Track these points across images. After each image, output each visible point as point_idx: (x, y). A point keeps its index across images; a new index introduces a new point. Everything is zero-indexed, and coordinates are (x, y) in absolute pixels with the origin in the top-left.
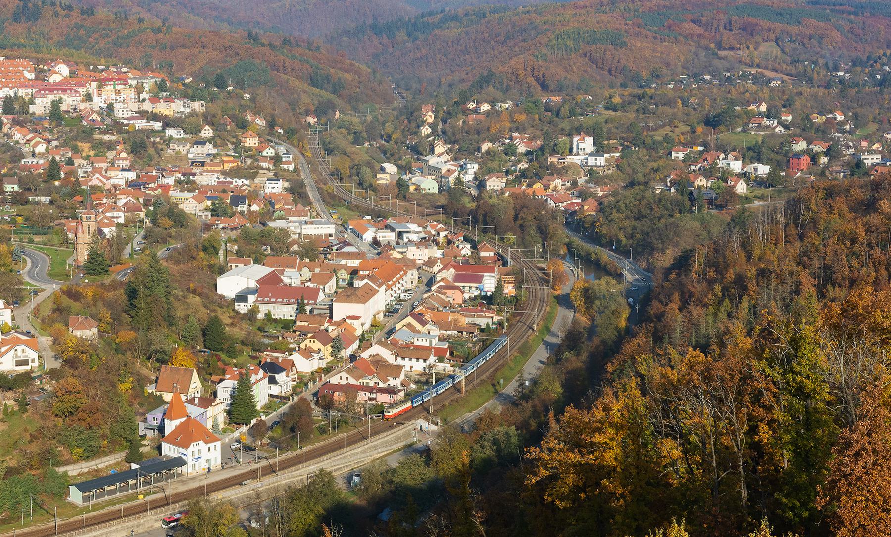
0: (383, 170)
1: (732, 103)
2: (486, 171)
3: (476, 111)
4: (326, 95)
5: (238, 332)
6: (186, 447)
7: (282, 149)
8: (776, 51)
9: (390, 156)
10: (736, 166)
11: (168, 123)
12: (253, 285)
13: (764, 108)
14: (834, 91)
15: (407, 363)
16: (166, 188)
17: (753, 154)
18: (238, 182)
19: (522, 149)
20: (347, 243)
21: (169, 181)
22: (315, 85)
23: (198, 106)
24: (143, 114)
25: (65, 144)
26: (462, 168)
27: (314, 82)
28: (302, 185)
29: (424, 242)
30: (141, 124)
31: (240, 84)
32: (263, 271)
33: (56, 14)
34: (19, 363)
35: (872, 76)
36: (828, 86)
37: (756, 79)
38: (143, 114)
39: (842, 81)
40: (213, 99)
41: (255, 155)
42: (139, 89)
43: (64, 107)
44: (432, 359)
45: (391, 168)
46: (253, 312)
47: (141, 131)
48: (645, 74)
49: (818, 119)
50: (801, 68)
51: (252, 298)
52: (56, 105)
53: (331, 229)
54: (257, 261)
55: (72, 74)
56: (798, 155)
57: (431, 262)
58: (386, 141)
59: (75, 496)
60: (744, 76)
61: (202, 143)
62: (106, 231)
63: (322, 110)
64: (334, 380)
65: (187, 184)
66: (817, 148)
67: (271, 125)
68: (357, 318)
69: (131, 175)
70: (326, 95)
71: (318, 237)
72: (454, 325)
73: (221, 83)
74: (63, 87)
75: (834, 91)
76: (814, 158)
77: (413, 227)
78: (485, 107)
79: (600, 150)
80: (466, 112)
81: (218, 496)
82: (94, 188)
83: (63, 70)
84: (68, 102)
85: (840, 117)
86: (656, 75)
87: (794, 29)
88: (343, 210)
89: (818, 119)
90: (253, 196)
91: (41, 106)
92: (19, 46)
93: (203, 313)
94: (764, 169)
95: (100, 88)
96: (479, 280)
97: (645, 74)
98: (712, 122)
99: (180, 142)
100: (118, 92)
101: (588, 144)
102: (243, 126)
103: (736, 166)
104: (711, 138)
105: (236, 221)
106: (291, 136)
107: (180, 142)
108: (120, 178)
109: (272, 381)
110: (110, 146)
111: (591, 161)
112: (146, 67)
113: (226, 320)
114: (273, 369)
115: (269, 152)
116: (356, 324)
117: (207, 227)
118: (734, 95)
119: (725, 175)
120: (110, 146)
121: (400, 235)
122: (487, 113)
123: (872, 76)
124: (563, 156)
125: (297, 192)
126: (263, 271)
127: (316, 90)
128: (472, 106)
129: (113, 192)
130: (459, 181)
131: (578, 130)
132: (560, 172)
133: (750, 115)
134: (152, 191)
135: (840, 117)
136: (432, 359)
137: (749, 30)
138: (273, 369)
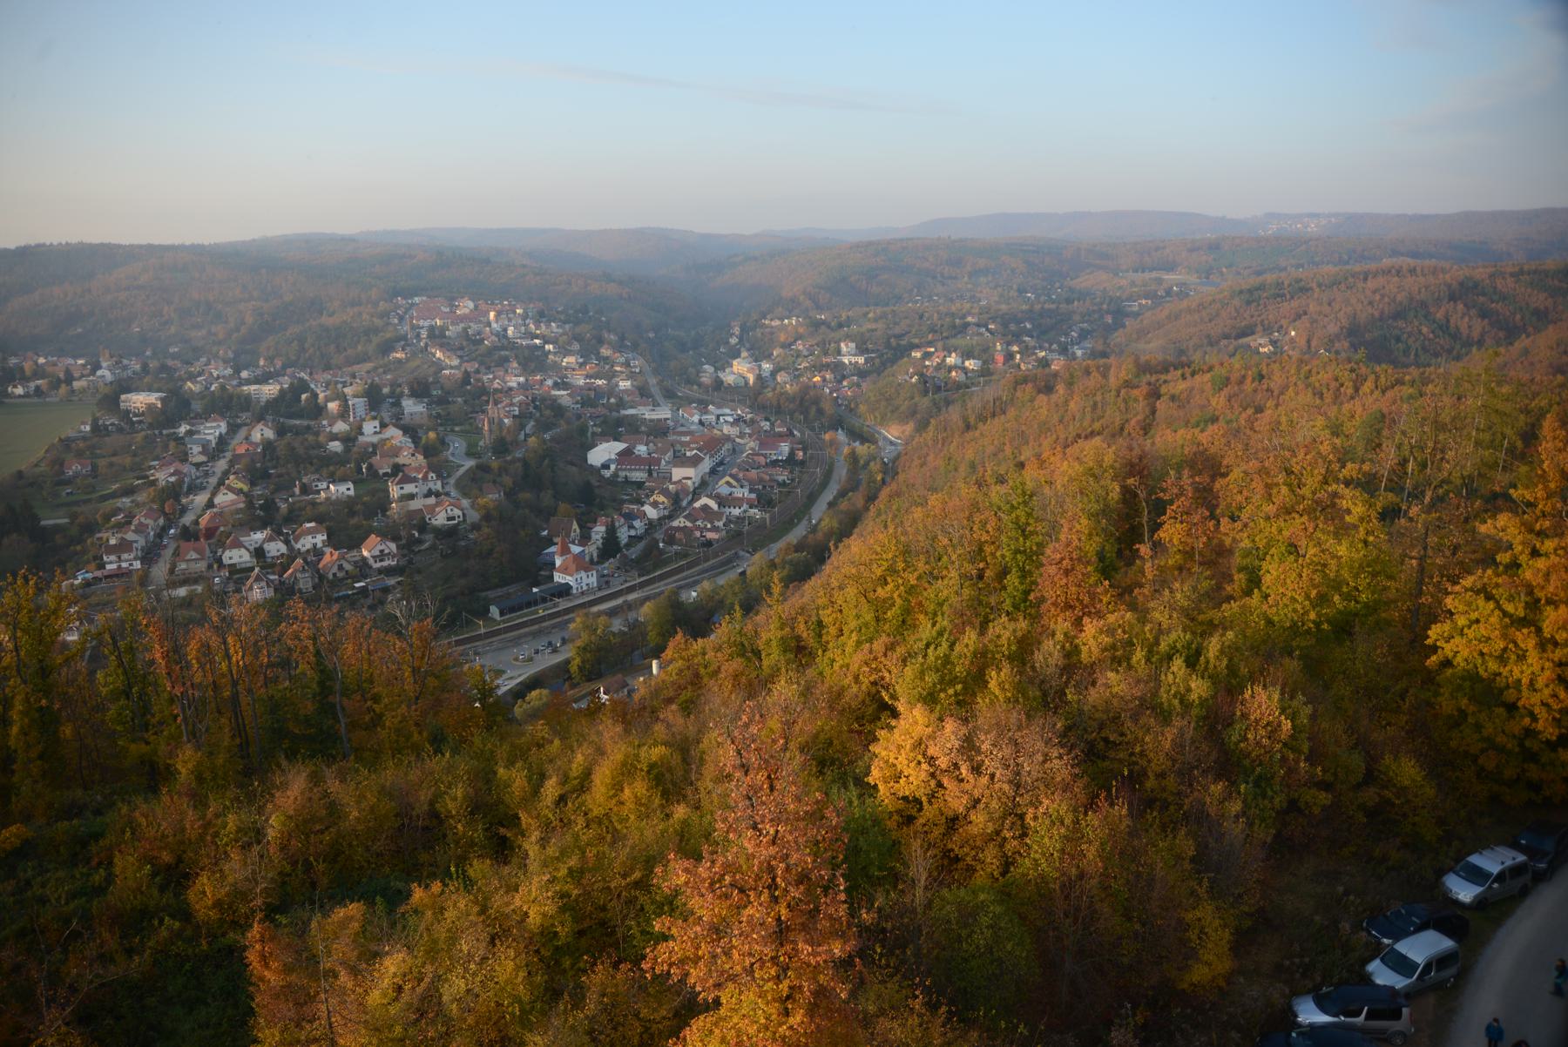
32: (620, 446)
46: (615, 475)
51: (613, 467)
64: (675, 523)
67: (622, 339)
77: (727, 411)
114: (630, 517)
126: (620, 446)
136: (745, 506)
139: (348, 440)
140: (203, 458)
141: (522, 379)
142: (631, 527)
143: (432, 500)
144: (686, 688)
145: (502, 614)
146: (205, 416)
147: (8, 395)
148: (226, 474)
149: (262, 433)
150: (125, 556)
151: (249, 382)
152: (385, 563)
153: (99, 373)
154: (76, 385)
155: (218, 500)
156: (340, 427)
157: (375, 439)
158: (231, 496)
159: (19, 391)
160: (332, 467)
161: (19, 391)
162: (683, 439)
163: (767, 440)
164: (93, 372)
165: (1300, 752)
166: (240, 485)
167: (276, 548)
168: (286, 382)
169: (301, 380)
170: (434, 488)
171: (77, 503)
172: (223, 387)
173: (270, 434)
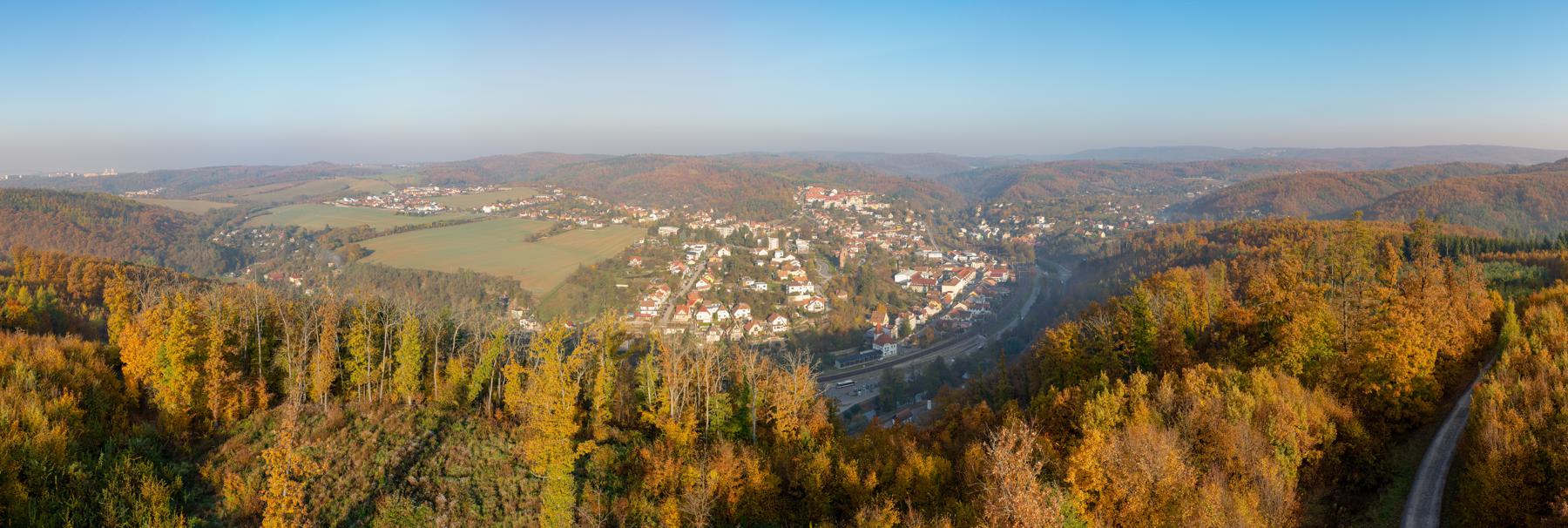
0: (961, 231)
1: (1097, 202)
2: (1002, 232)
3: (997, 207)
4: (938, 201)
5: (902, 297)
6: (882, 345)
7: (920, 223)
8: (1112, 182)
9: (963, 226)
10: (1101, 226)
11: (876, 212)
12: (909, 278)
13: (1110, 204)
14: (1135, 197)
15: (973, 311)
16: (874, 238)
17: (1106, 222)
18: (902, 236)
19: (1017, 222)
20: (946, 261)
21: (876, 235)
22: (934, 197)
23: (887, 206)
24: (865, 209)
25: (835, 220)
26: (993, 230)
27: (932, 195)
28: (928, 237)
29: (978, 261)
30: (865, 213)
31: (903, 196)
32: (913, 272)
33: (832, 170)
34: (817, 308)
35: (1148, 190)
36: (1132, 195)
37: (1105, 193)
38: (865, 209)
39: (1138, 192)
40: (892, 202)
41: (909, 225)
42: (864, 199)
43: (836, 206)
44: (983, 309)
45: (964, 230)
46: (910, 288)
47: (865, 215)
48: (1063, 192)
49: (1130, 208)
50: (1122, 188)
51: (909, 284)
52: (832, 205)
53: (940, 255)
54: (911, 268)
55: (838, 193)
56: (1124, 222)
57: (981, 268)
58: (948, 272)
59: (838, 364)
60: (1101, 192)
61: (889, 220)
62: (851, 255)
63: (936, 207)
64: (943, 318)
65: (882, 237)
66: (1130, 219)
67: (916, 213)
68: (951, 292)
69: (861, 233)
70: (938, 201)
71: (935, 258)
72: (992, 294)
73: (896, 196)
74: (835, 198)
75: (1135, 197)
76: (1130, 222)
77: (974, 254)
78: (1001, 205)
79: (1047, 222)
80: (993, 207)
81: (896, 366)
82: (847, 238)
83: (835, 191)
84: (837, 204)
85: (1138, 207)
86: (1068, 192)
87: (1119, 173)
88: (946, 248)
89: (1130, 208)
90: (909, 242)
91: (827, 205)
92: (819, 182)
93: (889, 290)
94: (1111, 227)
95: (849, 198)
96: (1001, 275)
97: (1063, 192)
98: (1089, 209)
99: (881, 220)
100: (856, 200)
101: (1042, 220)
102: (905, 214)
103: (1101, 226)
104: (1091, 216)
105: (902, 252)
106: (924, 217)
107: (881, 220)
108: (856, 234)
109: (918, 318)
110: (853, 221)
111: (1044, 226)
112: (866, 191)
113: (898, 292)
114: (917, 313)
115: (915, 224)
116: (952, 294)
117: (890, 254)
118: (1098, 199)
119: (1097, 231)
120: (853, 221)
121: (969, 258)
122: (1002, 208)
123: (1148, 190)
124: (1033, 224)
125: (927, 241)
126: (913, 272)
127: (933, 199)
128: (996, 205)
129: (854, 240)
130: (991, 235)
131: (1038, 214)
132: (1032, 231)
133: (1105, 207)
134: (869, 239)
135: (1138, 207)
136: (983, 309)
137: (1102, 174)
138: (917, 313)
139: (768, 259)
140: (693, 263)
141: (861, 233)
142: (918, 318)
143: (808, 297)
144: (952, 420)
145: (842, 366)
146: (696, 240)
147: (612, 223)
148: (703, 272)
149: (725, 252)
150: (650, 308)
151: (719, 225)
152: (780, 330)
153: (651, 216)
154: (640, 220)
155: (698, 285)
156: (764, 253)
157: (781, 261)
158: (704, 284)
159: (616, 221)
160: (758, 275)
161: (616, 221)
162: (949, 269)
163: (997, 271)
164: (648, 216)
165: (1304, 429)
166: (709, 278)
167: (723, 315)
168: (738, 226)
169: (745, 226)
170: (810, 290)
171: (633, 278)
172: (706, 227)
173: (728, 253)
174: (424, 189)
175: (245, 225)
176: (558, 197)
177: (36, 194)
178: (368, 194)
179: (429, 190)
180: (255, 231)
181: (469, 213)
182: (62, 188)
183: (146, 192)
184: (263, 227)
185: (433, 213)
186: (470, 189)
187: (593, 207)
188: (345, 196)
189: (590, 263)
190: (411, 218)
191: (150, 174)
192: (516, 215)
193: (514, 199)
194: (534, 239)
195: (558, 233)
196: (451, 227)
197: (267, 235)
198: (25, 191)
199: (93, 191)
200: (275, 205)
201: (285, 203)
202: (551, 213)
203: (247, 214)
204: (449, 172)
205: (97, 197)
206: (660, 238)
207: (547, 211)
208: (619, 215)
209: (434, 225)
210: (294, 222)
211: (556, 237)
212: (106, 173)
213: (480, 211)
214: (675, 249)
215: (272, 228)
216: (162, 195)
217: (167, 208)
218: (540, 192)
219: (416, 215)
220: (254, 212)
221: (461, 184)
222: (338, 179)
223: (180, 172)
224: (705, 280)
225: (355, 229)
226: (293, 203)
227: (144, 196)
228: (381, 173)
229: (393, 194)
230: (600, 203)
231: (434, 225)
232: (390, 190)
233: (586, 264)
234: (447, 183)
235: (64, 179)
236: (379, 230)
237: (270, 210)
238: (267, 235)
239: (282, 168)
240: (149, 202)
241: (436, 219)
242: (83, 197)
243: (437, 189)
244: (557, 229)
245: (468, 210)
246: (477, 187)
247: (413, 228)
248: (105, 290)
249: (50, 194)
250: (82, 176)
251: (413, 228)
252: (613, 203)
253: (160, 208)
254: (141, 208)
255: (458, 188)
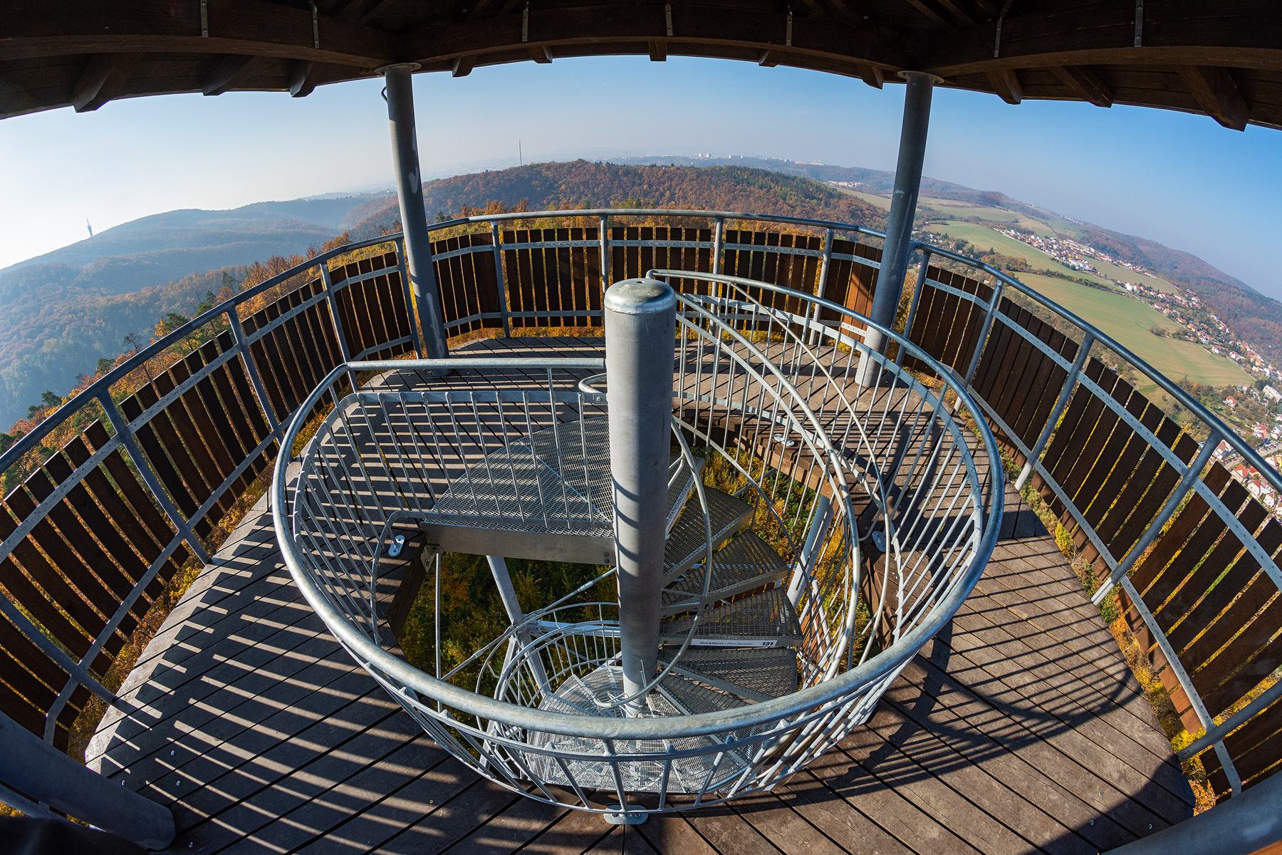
154: (1254, 368)
161: (1233, 356)
174: (1081, 246)
175: (924, 229)
176: (1193, 305)
177: (755, 173)
178: (1032, 233)
179: (1085, 249)
180: (931, 236)
181: (1113, 283)
182: (776, 170)
183: (846, 184)
184: (938, 234)
185: (1080, 269)
186: (1121, 262)
187: (1220, 331)
188: (1013, 229)
189: (1195, 382)
190: (1062, 266)
191: (851, 170)
192: (1152, 304)
193: (1156, 289)
194: (1160, 334)
195: (1180, 338)
196: (1084, 286)
197: (941, 241)
198: (745, 169)
199: (802, 176)
200: (952, 218)
201: (961, 219)
202: (1182, 317)
203: (928, 220)
204: (1107, 239)
205: (804, 181)
206: (1262, 395)
207: (1179, 314)
208: (1238, 351)
209: (1080, 282)
210: (965, 238)
211: (1177, 341)
212: (814, 163)
213: (1123, 286)
214: (1269, 414)
215: (946, 237)
216: (860, 189)
217: (862, 200)
218: (1180, 292)
219: (1068, 266)
220: (934, 219)
221: (1115, 254)
222: (1011, 212)
223: (877, 172)
224: (1275, 460)
225: (1013, 259)
226: (967, 221)
227: (843, 187)
228: (1048, 219)
229: (1054, 241)
230: (1227, 331)
231: (1080, 282)
232: (1053, 236)
233: (1190, 379)
234: (1103, 249)
235: (777, 163)
236: (1034, 268)
237: (947, 222)
238: (941, 241)
239: (965, 189)
240: (849, 193)
241: (1084, 277)
242: (794, 179)
243: (1093, 250)
244: (1181, 335)
245: (1113, 281)
246: (1127, 263)
247: (1061, 276)
248: (1101, 808)
249: (767, 174)
250: (793, 163)
251: (1061, 276)
252: (1239, 337)
253: (856, 198)
254: (840, 196)
255: (1111, 256)
